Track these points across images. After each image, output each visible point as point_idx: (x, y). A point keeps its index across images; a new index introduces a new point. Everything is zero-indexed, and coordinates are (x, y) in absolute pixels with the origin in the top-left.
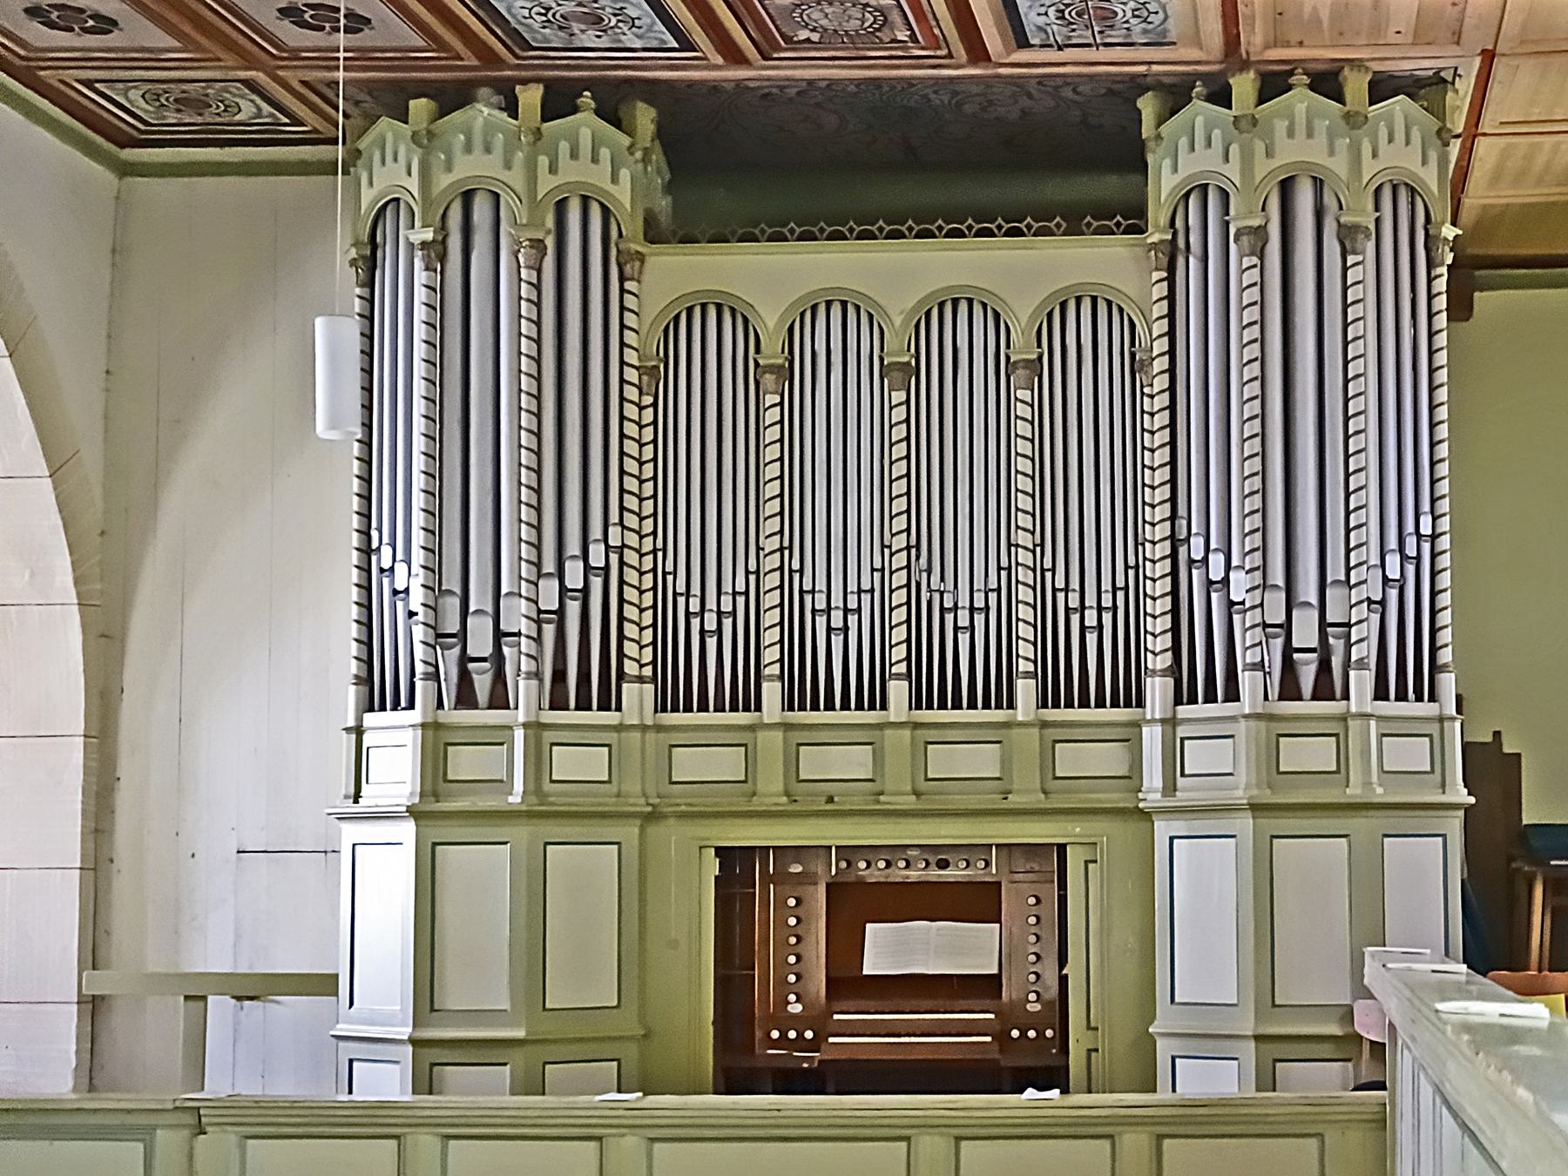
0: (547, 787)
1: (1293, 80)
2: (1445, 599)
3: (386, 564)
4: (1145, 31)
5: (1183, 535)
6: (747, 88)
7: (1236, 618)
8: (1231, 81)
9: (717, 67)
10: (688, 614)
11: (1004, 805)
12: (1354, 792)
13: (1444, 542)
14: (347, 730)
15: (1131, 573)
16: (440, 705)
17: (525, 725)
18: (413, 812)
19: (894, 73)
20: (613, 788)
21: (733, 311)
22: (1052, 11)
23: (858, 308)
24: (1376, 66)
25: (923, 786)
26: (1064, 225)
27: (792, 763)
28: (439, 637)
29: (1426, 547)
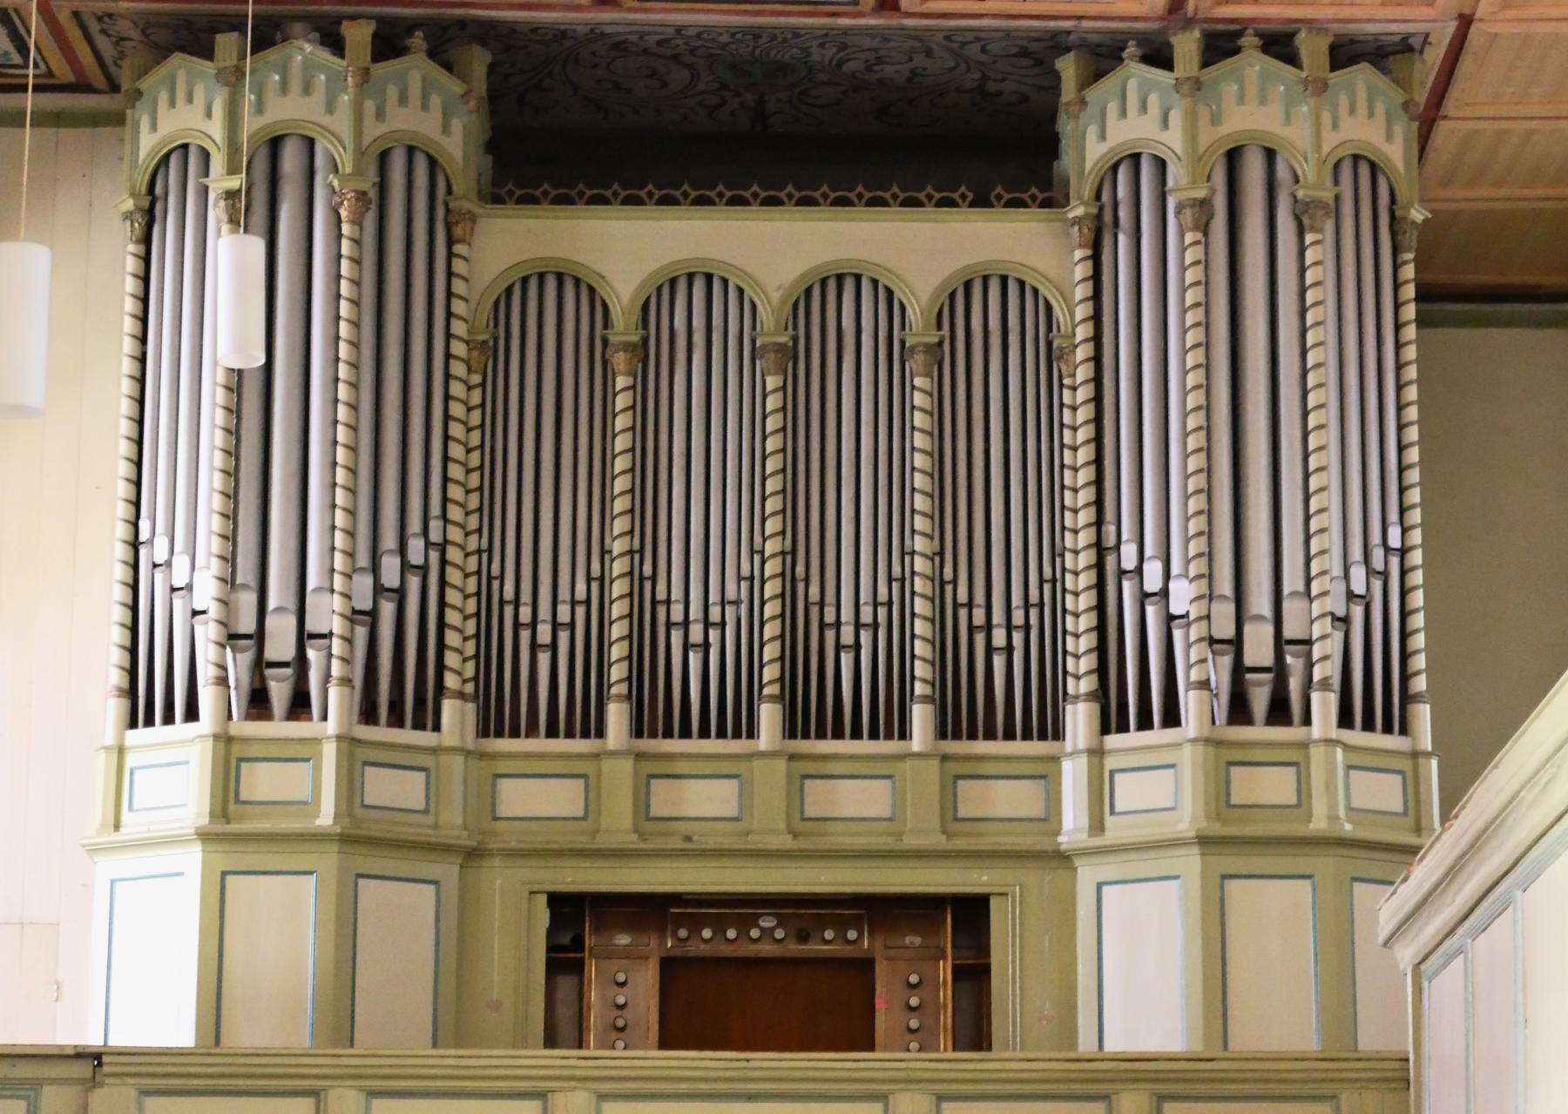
0: (358, 811)
2: (1418, 621)
3: (160, 557)
6: (602, 34)
7: (1178, 635)
8: (1173, 40)
11: (898, 846)
12: (1319, 824)
13: (1416, 557)
14: (106, 748)
15: (1047, 587)
16: (230, 717)
17: (339, 738)
18: (205, 836)
19: (782, 20)
20: (430, 819)
21: (577, 281)
23: (725, 282)
26: (971, 196)
29: (1395, 562)
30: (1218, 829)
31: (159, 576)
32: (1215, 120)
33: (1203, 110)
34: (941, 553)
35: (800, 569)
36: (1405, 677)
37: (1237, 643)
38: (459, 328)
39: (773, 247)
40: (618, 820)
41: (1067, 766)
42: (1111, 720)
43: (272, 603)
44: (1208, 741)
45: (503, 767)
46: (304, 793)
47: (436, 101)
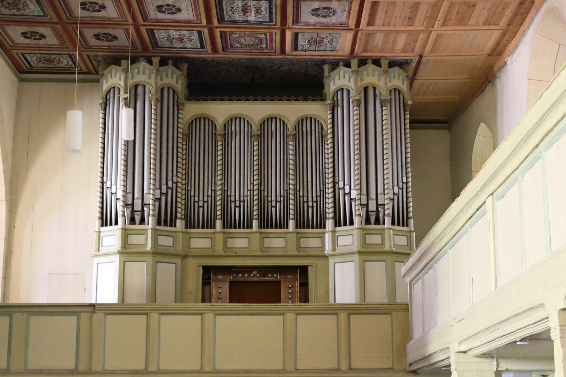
1: (368, 61)
4: (331, 47)
7: (353, 203)
9: (209, 54)
10: (194, 202)
12: (387, 248)
13: (410, 184)
15: (322, 192)
17: (152, 229)
22: (307, 41)
23: (244, 119)
25: (263, 250)
28: (126, 205)
29: (405, 185)
30: (363, 250)
32: (361, 80)
33: (359, 78)
36: (407, 213)
37: (367, 205)
38: (180, 130)
39: (256, 111)
40: (219, 249)
41: (327, 235)
42: (337, 224)
44: (361, 229)
46: (144, 242)
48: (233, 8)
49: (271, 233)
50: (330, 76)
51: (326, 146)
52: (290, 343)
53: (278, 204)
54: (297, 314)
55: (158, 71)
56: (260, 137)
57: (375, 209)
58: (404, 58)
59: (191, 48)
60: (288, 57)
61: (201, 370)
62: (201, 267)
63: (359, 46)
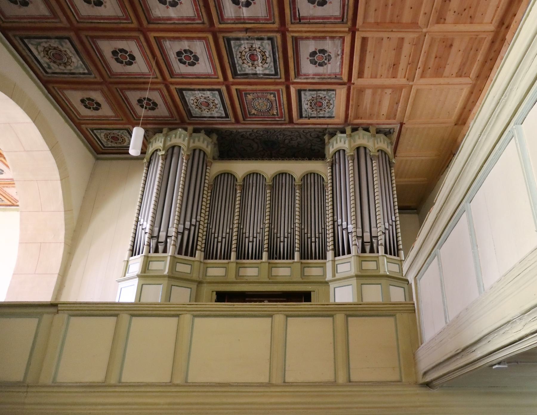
0: (174, 272)
5: (336, 220)
7: (350, 236)
11: (291, 281)
12: (382, 272)
13: (398, 222)
16: (150, 252)
17: (171, 256)
24: (378, 126)
27: (237, 272)
28: (152, 237)
29: (394, 223)
30: (359, 274)
31: (141, 227)
32: (354, 142)
33: (352, 141)
34: (302, 223)
35: (273, 226)
36: (398, 246)
37: (362, 237)
38: (207, 181)
39: (269, 168)
40: (232, 277)
41: (328, 264)
42: (337, 254)
43: (162, 230)
44: (357, 256)
45: (208, 266)
46: (162, 268)
47: (206, 142)
48: (241, 53)
49: (279, 263)
50: (329, 143)
51: (327, 201)
52: (279, 349)
53: (286, 239)
54: (287, 316)
55: (191, 135)
56: (272, 187)
57: (369, 240)
58: (388, 126)
59: (218, 117)
60: (296, 126)
61: (170, 382)
62: (215, 293)
63: (352, 111)
